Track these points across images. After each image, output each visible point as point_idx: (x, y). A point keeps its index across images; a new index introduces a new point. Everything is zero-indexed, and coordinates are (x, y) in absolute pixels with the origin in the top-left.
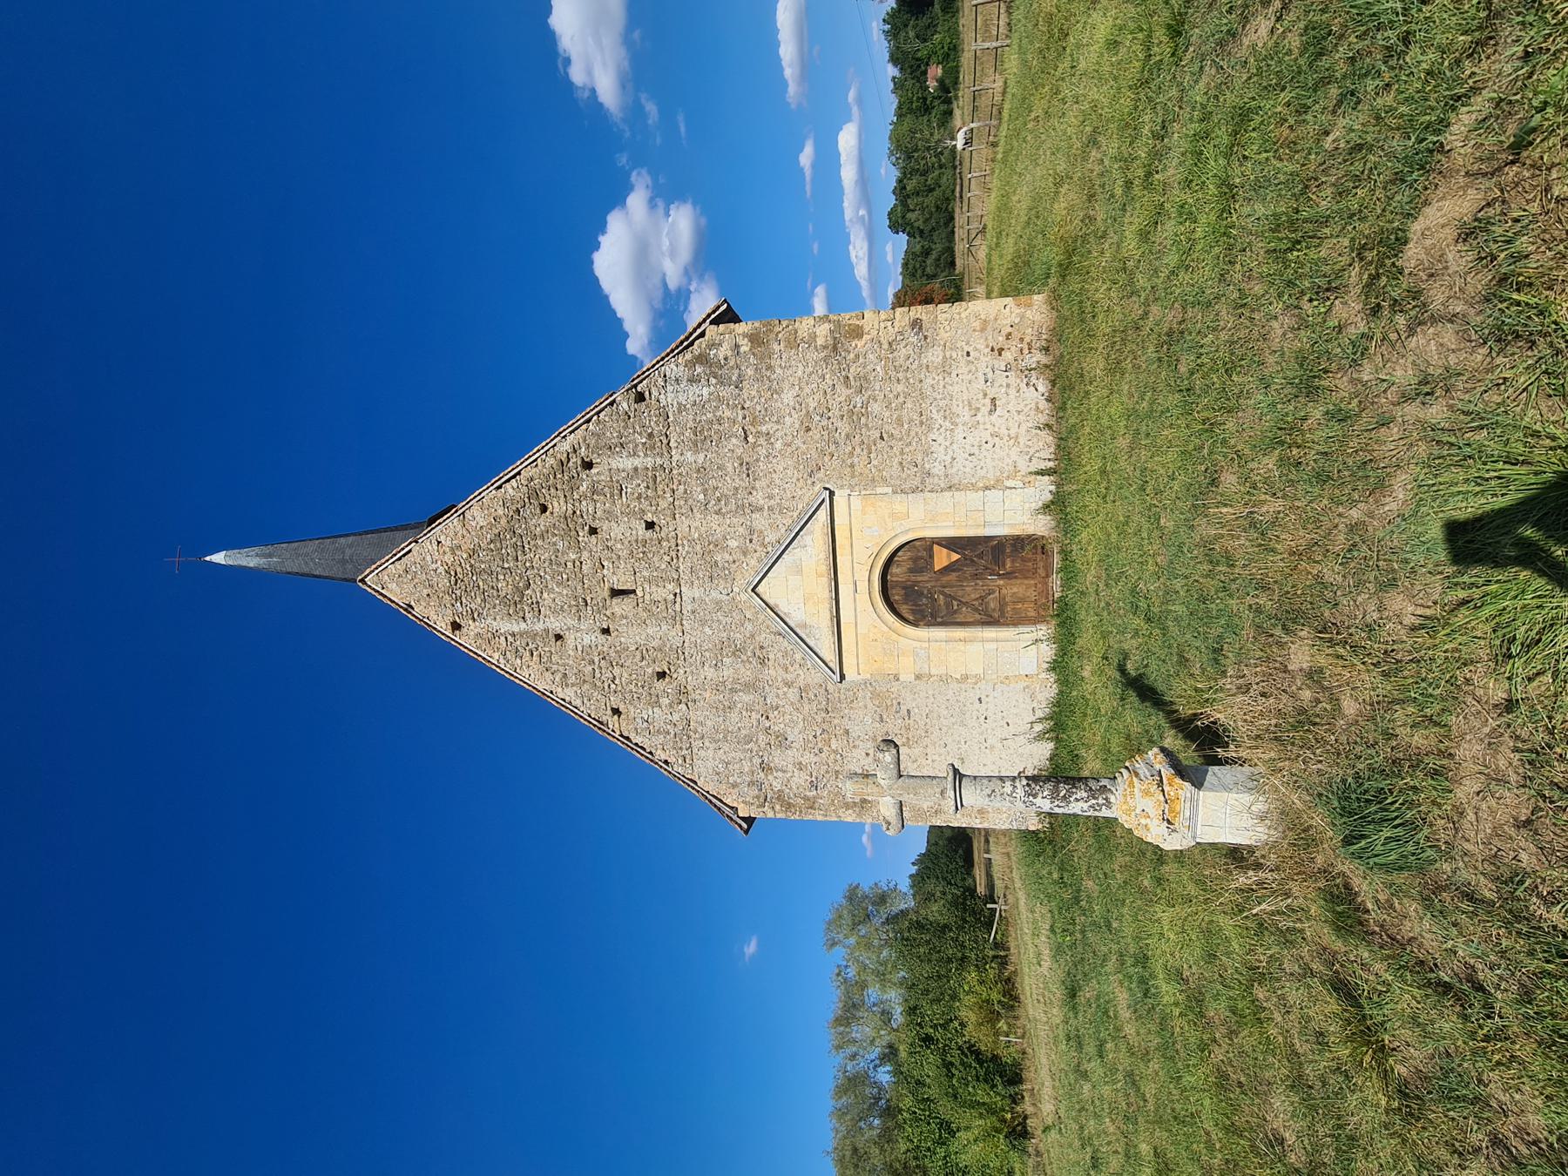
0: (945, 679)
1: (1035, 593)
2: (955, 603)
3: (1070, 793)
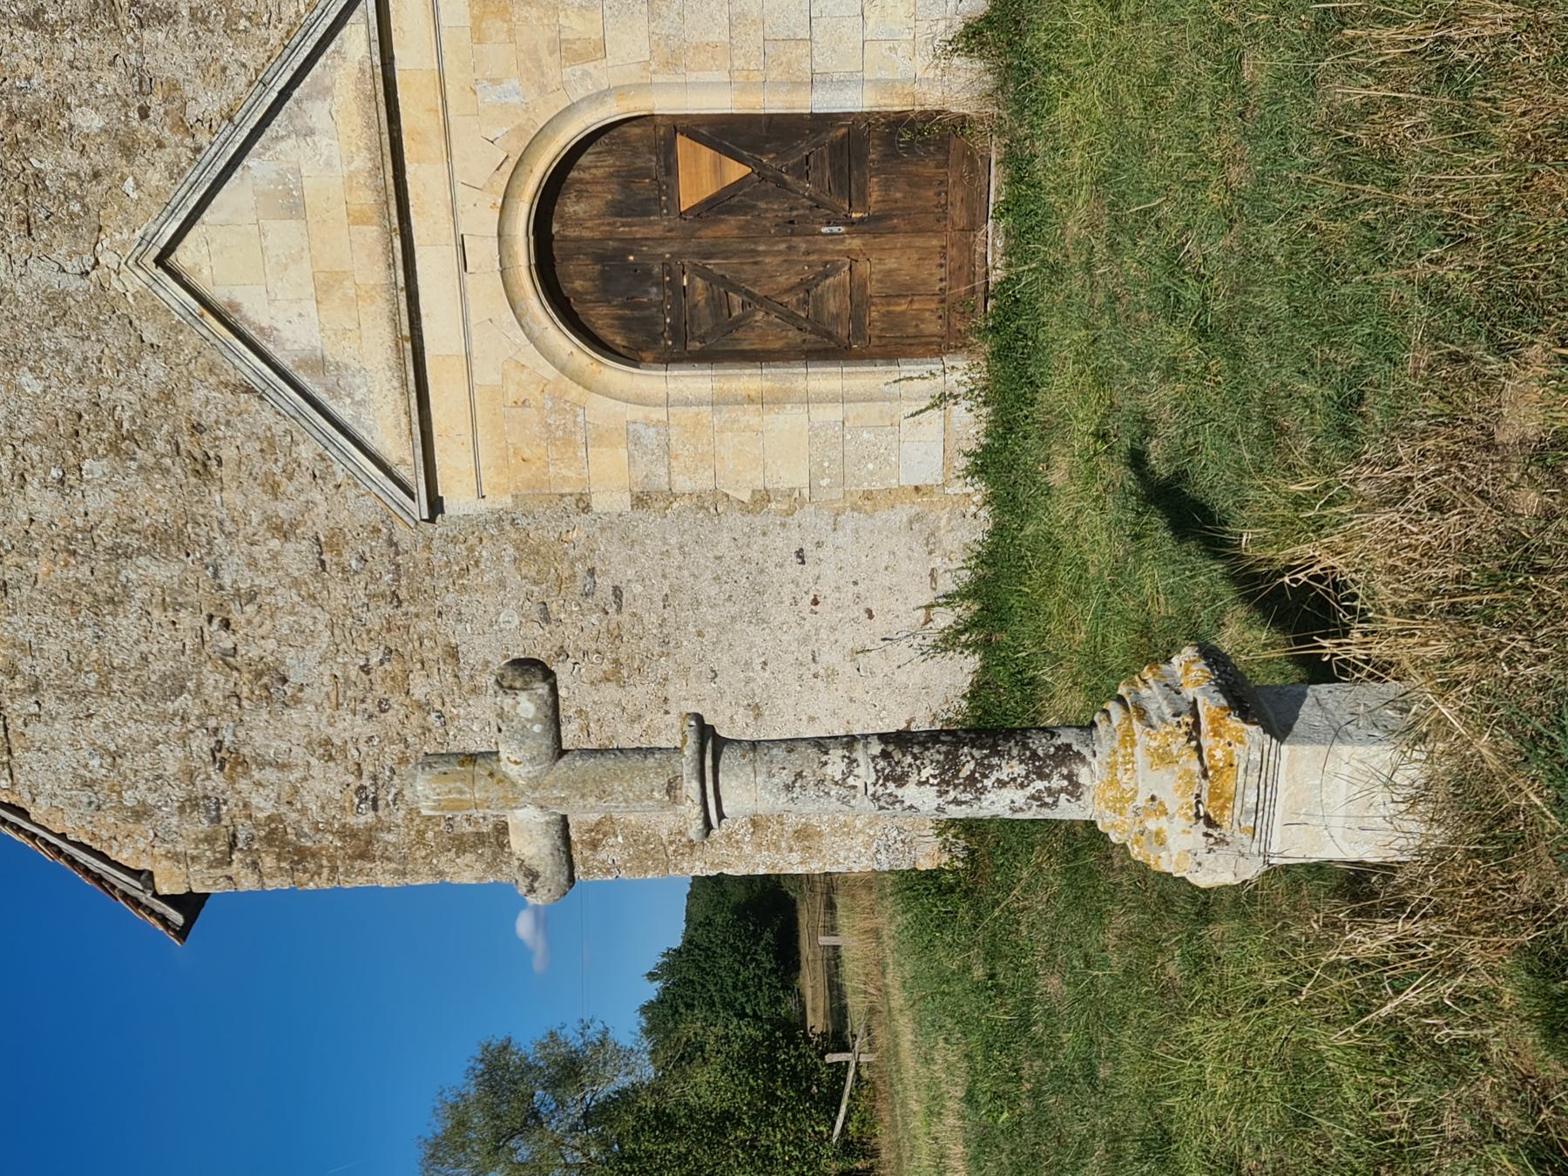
0: (710, 503)
1: (942, 272)
2: (736, 299)
3: (985, 768)
